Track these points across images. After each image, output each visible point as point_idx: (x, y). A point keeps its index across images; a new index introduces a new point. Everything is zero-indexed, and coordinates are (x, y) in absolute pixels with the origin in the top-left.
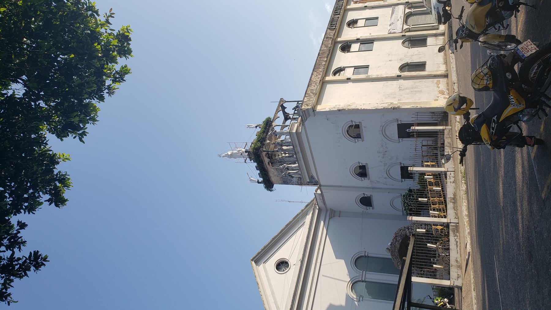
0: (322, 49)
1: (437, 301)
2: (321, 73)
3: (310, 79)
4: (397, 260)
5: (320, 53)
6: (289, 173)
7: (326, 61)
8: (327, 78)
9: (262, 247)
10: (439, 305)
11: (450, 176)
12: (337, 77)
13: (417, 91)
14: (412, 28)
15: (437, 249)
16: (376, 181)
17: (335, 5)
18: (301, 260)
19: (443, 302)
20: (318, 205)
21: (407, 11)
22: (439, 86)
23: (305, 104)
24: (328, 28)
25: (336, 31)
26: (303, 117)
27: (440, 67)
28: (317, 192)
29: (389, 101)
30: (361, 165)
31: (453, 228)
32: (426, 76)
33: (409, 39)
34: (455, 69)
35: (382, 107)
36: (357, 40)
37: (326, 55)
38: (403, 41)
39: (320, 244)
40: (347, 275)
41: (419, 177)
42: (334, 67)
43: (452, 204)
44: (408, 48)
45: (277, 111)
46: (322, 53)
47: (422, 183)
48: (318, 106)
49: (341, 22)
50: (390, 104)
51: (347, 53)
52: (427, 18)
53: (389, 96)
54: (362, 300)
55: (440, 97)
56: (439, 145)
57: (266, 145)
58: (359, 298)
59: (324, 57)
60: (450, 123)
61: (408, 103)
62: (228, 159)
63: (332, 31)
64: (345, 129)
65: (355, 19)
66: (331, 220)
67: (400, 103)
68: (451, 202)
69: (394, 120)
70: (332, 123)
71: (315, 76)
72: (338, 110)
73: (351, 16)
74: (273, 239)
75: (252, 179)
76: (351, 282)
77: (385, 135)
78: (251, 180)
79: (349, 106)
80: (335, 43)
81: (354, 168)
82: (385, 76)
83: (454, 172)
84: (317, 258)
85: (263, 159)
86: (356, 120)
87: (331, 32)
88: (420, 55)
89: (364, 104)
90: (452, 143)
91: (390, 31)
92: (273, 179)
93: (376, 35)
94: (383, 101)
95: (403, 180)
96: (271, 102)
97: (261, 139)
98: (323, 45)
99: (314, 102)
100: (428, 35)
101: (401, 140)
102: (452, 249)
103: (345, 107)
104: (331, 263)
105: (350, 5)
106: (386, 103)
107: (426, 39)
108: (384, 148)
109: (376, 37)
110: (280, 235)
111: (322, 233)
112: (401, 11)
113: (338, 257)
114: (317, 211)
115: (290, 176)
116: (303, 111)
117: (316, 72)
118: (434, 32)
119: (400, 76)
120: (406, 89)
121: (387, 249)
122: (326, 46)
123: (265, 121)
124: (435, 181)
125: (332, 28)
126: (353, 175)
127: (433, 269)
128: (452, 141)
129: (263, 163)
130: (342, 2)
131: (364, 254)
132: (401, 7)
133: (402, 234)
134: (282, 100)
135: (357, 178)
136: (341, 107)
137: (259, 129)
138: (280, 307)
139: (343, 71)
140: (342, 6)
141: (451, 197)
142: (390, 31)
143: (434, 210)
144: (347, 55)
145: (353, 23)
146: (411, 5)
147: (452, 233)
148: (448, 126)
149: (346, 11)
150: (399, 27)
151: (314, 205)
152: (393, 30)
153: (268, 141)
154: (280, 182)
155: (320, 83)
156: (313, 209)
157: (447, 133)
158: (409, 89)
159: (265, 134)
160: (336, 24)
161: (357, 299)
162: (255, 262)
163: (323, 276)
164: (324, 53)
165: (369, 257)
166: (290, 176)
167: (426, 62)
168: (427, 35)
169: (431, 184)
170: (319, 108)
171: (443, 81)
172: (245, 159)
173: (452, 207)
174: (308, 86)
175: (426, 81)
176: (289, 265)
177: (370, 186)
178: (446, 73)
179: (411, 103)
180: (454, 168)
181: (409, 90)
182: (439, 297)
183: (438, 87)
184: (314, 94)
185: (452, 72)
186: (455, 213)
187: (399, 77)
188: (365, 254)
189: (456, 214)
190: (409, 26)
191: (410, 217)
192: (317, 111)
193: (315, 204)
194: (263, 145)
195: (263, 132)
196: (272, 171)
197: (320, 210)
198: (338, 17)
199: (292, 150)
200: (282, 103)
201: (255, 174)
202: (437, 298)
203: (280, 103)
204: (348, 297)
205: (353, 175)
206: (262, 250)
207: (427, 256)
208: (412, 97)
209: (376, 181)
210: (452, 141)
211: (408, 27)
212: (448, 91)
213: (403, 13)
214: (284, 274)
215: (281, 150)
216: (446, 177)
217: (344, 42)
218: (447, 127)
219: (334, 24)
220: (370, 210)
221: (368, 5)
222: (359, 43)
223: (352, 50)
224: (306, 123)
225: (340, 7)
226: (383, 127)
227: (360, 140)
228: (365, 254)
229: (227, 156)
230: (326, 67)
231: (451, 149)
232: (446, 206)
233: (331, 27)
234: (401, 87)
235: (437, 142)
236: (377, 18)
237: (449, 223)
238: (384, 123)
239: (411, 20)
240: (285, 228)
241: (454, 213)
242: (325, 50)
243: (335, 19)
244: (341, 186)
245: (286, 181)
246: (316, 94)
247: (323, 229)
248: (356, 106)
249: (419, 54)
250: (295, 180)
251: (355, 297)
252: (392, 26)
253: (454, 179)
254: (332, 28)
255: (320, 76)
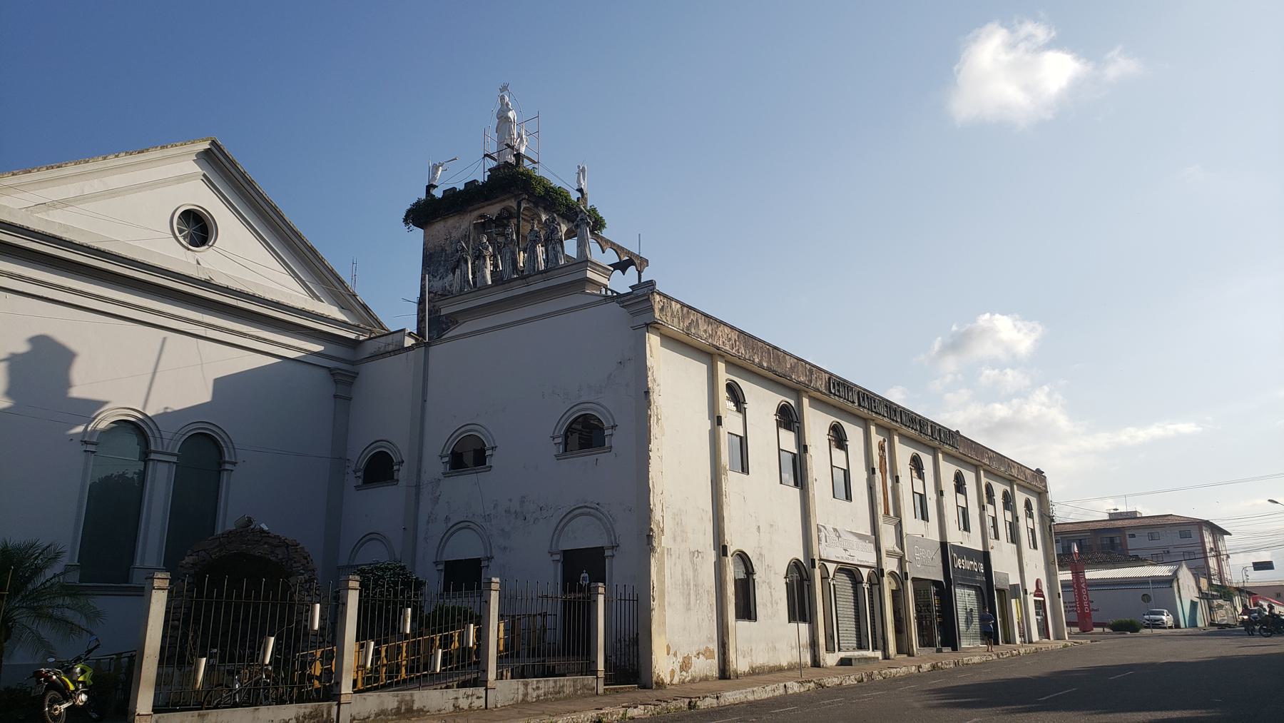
0: (788, 357)
1: (78, 670)
2: (734, 351)
3: (721, 322)
4: (214, 548)
5: (779, 352)
6: (466, 262)
7: (761, 366)
8: (721, 366)
9: (251, 175)
10: (67, 680)
11: (472, 695)
12: (723, 394)
13: (690, 599)
14: (829, 584)
15: (249, 665)
16: (440, 495)
17: (878, 396)
18: (213, 282)
19: (77, 689)
20: (370, 339)
21: (865, 573)
22: (701, 656)
23: (664, 302)
24: (831, 374)
25: (825, 394)
26: (632, 296)
27: (744, 657)
28: (407, 338)
29: (668, 525)
30: (488, 453)
31: (323, 712)
32: (725, 621)
33: (805, 577)
34: (751, 698)
35: (655, 505)
36: (803, 447)
37: (774, 366)
38: (801, 562)
39: (258, 339)
40: (167, 408)
41: (460, 609)
42: (746, 386)
43: (395, 707)
44: (787, 575)
45: (618, 249)
46: (778, 355)
47: (441, 616)
48: (659, 338)
49: (841, 410)
50: (661, 526)
51: (777, 420)
52: (848, 623)
53: (678, 524)
54: (85, 451)
55: (675, 659)
56: (550, 662)
57: (536, 210)
58: (92, 444)
59: (769, 362)
60: (611, 689)
61: (663, 573)
62: (495, 112)
63: (826, 384)
64: (595, 411)
65: (847, 443)
66: (323, 373)
67: (663, 554)
68: (400, 702)
69: (615, 539)
70: (611, 374)
71: (730, 336)
72: (649, 388)
73: (854, 433)
74: (274, 209)
75: (440, 172)
76: (140, 419)
77: (571, 515)
78: (436, 168)
79: (658, 419)
80: (797, 392)
81: (476, 434)
82: (726, 514)
83: (484, 707)
84: (217, 327)
85: (499, 199)
86: (617, 439)
87: (824, 383)
88: (771, 606)
89: (660, 457)
90: (560, 699)
91: (822, 529)
92: (440, 228)
93: (814, 494)
94: (667, 507)
95: (441, 567)
96: (639, 235)
97: (552, 200)
98: (796, 360)
99: (670, 326)
100: (815, 626)
101: (557, 557)
102: (257, 712)
103: (655, 408)
104: (202, 364)
105: (876, 433)
106: (663, 517)
107: (805, 621)
108: (534, 512)
109: (811, 495)
110: (285, 228)
111: (290, 346)
112: (864, 556)
113: (219, 384)
114: (353, 336)
115: (458, 261)
116: (649, 297)
117: (738, 338)
118: (822, 641)
119: (725, 554)
120: (695, 570)
121: (250, 521)
122: (792, 368)
123: (598, 215)
124: (452, 652)
125: (832, 385)
126: (459, 432)
127: (192, 657)
128: (565, 698)
129: (486, 200)
130: (886, 415)
131: (227, 459)
132: (872, 560)
133: (295, 562)
134: (645, 262)
135: (453, 438)
136: (654, 397)
137: (574, 196)
138: (65, 209)
139: (735, 408)
140: (876, 413)
141: (413, 701)
142: (822, 529)
143: (377, 652)
144: (772, 420)
145: (838, 438)
146: (876, 582)
147: (308, 711)
148: (605, 685)
149: (865, 423)
150: (831, 550)
151: (368, 328)
152: (826, 537)
153: (544, 218)
154: (430, 245)
155: (714, 346)
156: (358, 326)
157: (586, 682)
158: (694, 576)
159: (563, 209)
160: (839, 397)
161: (94, 431)
162: (207, 152)
163: (165, 339)
164: (779, 362)
165: (220, 473)
166: (458, 261)
167: (756, 620)
168: (815, 623)
169: (446, 642)
170: (653, 340)
171: (709, 666)
172: (495, 155)
173: (385, 707)
174: (706, 316)
175: (713, 621)
176: (198, 246)
177: (426, 478)
178: (732, 674)
179: (662, 582)
180: (496, 707)
181: (692, 577)
182: (93, 678)
183: (698, 654)
184: (688, 328)
185: (744, 691)
186: (368, 718)
187: (722, 550)
188: (228, 462)
189: (364, 719)
190: (834, 576)
191: (357, 585)
192: (647, 334)
193: (371, 332)
194: (534, 203)
195: (567, 206)
196: (461, 224)
197: (355, 344)
198: (853, 402)
199: (534, 270)
200: (636, 261)
201: (453, 178)
202: (89, 672)
203: (638, 257)
204: (94, 406)
205: (459, 432)
206: (243, 175)
207: (225, 634)
208: (676, 584)
209: (440, 495)
210: (565, 698)
211: (831, 576)
212: (689, 682)
213: (862, 561)
214: (170, 232)
215: (535, 239)
216: (463, 685)
217: (799, 414)
218: (601, 682)
219: (839, 391)
220: (353, 480)
221: (876, 475)
222: (795, 452)
223: (783, 432)
224: (614, 306)
225: (875, 407)
226: (597, 509)
227: (559, 448)
228: (228, 462)
229: (504, 109)
230: (747, 364)
231: (545, 695)
232: (384, 687)
233: (834, 384)
234: (698, 556)
235: (539, 656)
236: (849, 497)
237: (486, 686)
238: (608, 512)
239: (844, 582)
240: (305, 244)
241: (366, 715)
242: (784, 365)
243: (850, 394)
244: (425, 401)
245: (431, 261)
246: (688, 334)
247: (300, 349)
248: (656, 438)
249: (772, 604)
250: (435, 286)
251: (102, 426)
252: (833, 535)
253: (466, 707)
254: (832, 385)
255: (727, 348)
